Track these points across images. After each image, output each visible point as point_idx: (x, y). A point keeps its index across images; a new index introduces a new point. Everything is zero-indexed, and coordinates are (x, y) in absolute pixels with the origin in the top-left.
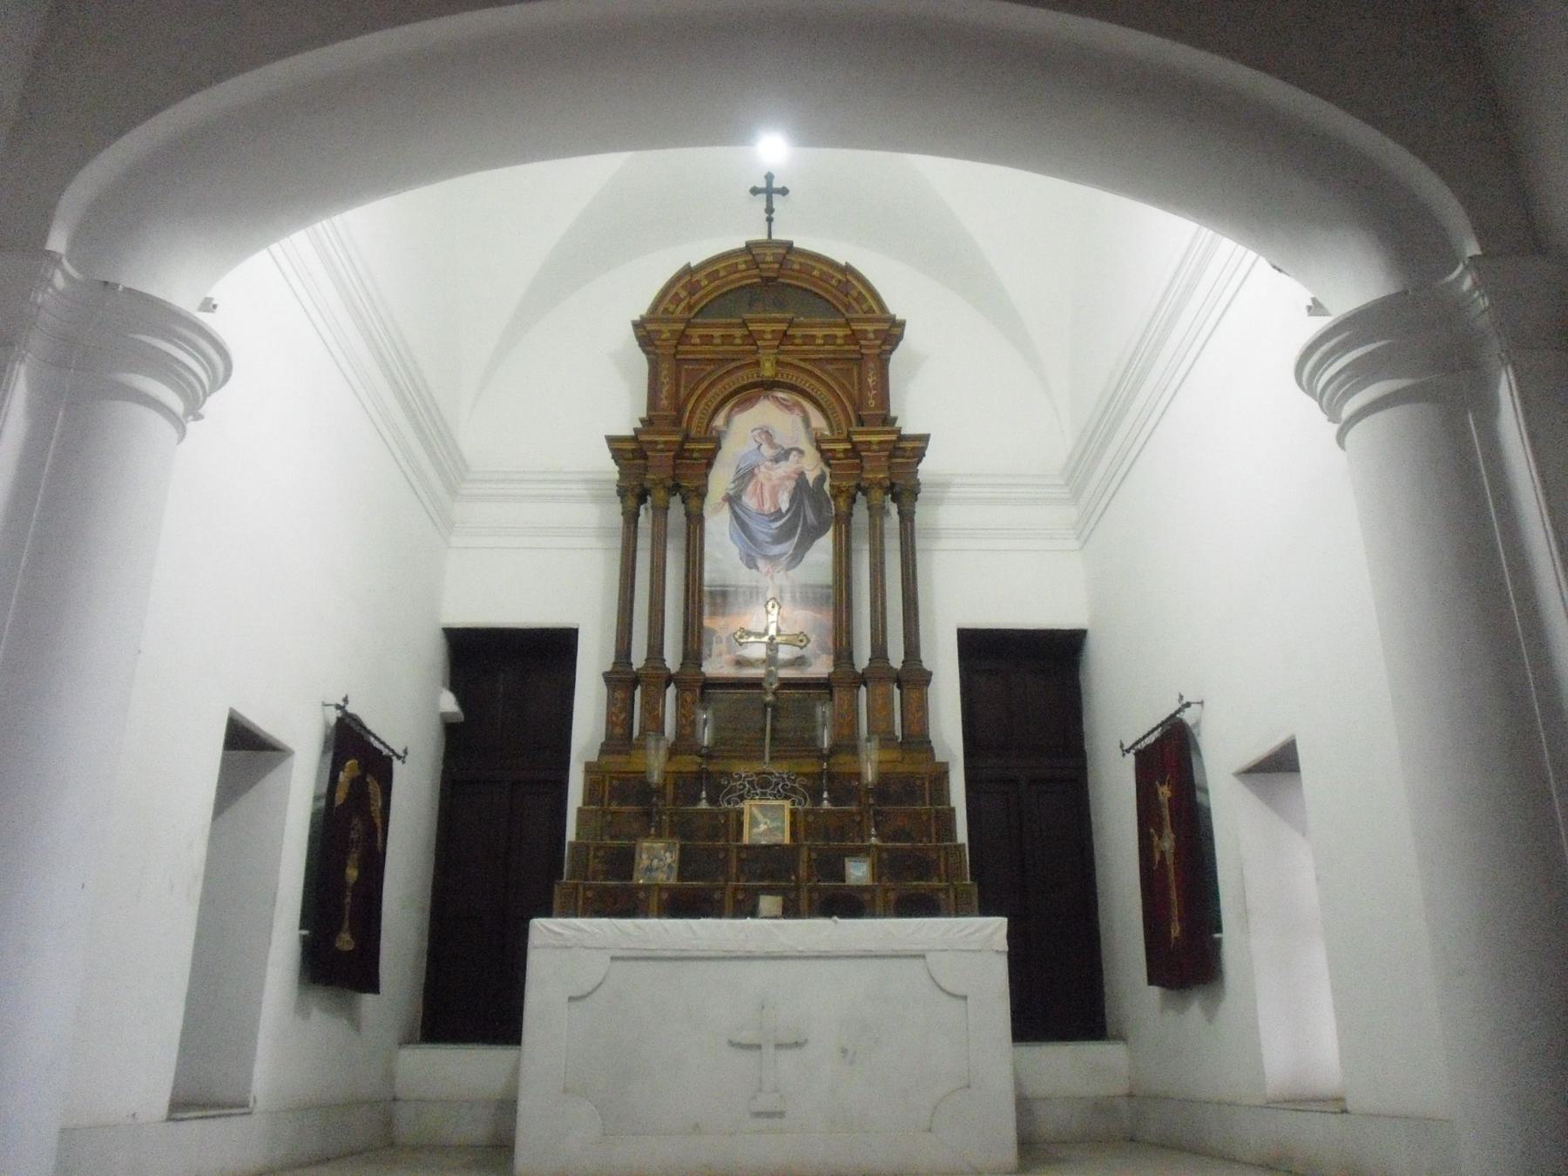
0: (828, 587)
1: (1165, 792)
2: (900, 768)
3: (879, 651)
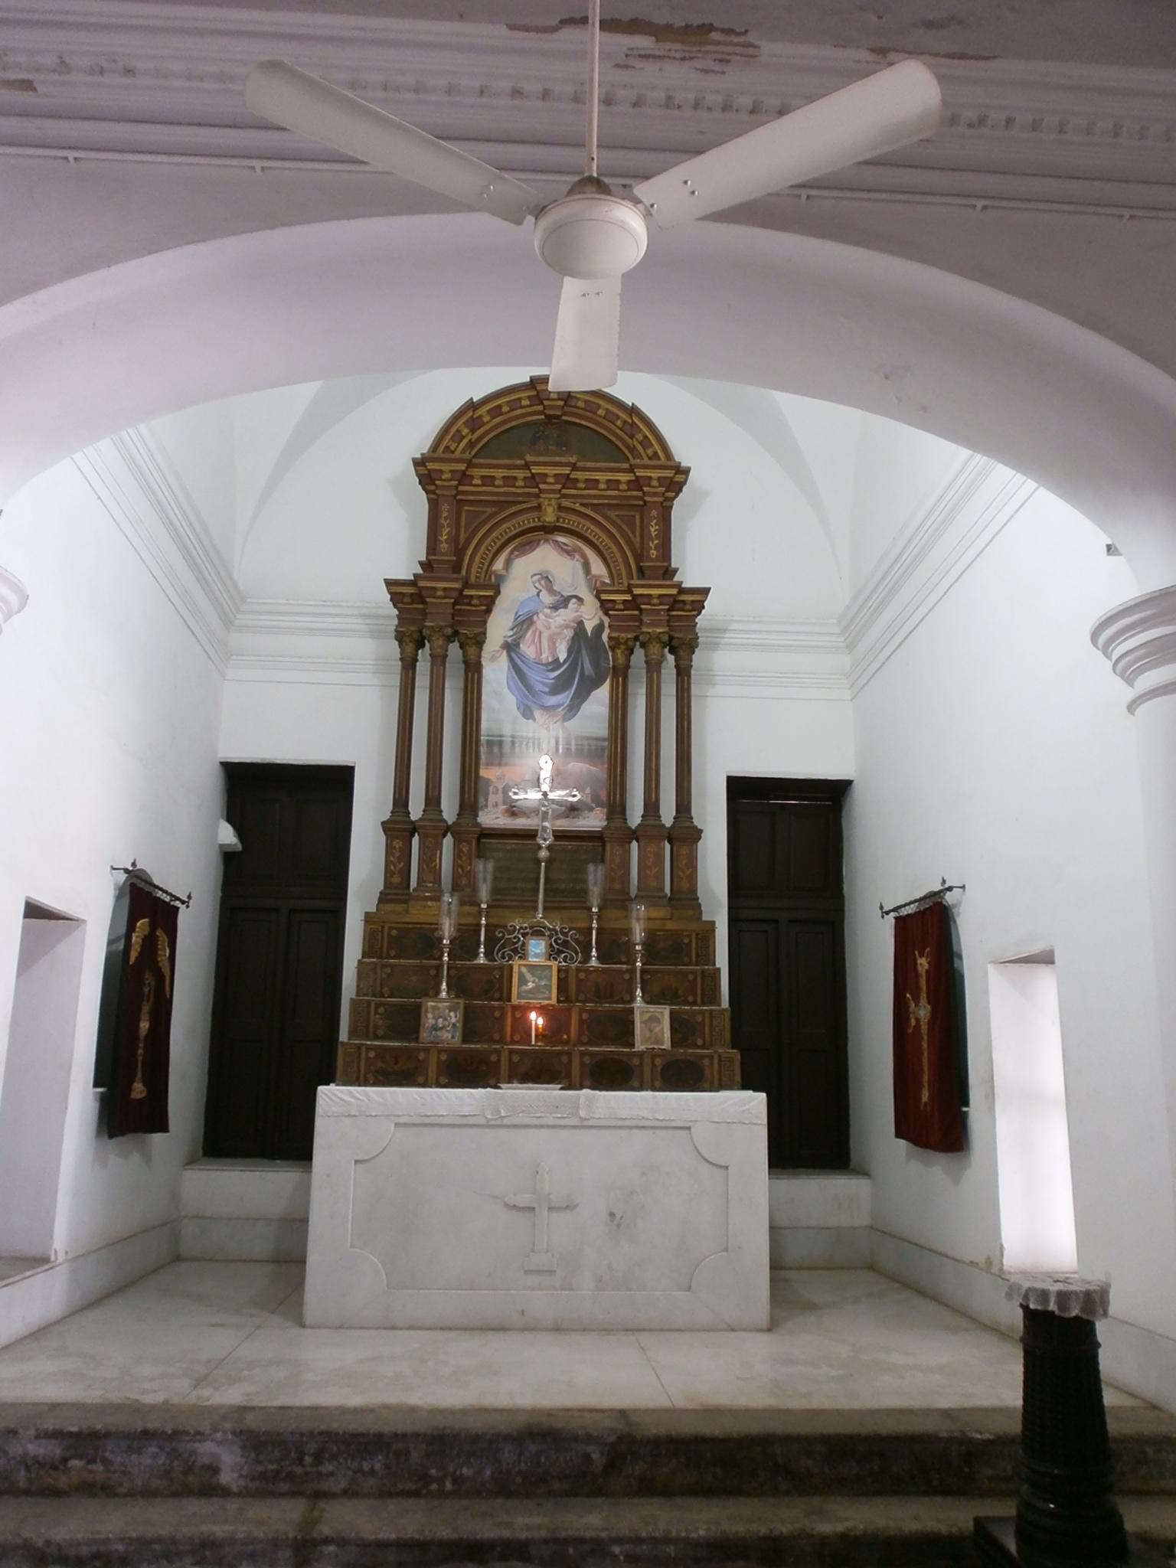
0: (603, 740)
1: (923, 964)
2: (671, 925)
3: (652, 807)
